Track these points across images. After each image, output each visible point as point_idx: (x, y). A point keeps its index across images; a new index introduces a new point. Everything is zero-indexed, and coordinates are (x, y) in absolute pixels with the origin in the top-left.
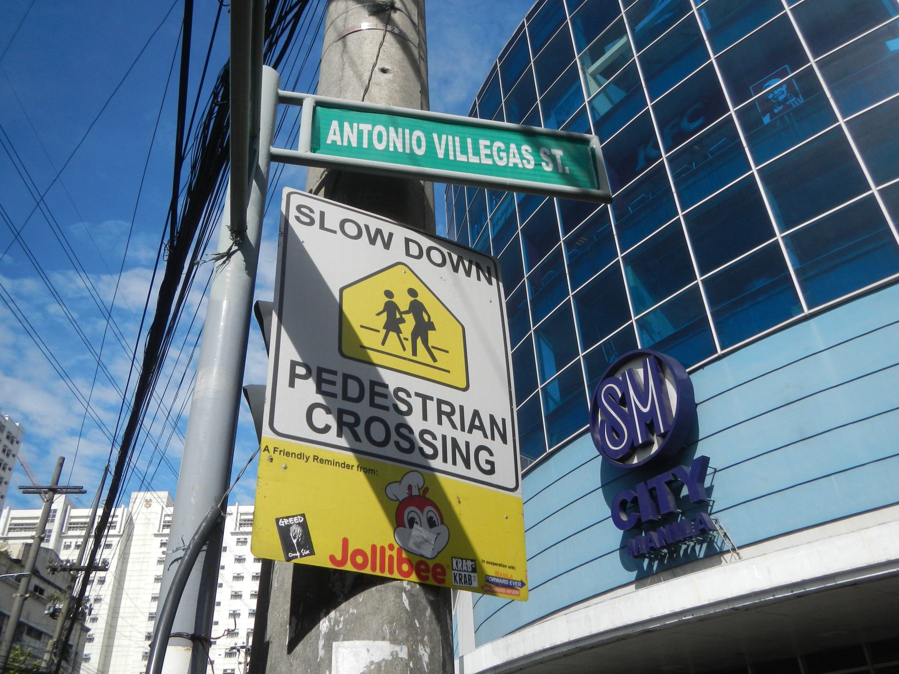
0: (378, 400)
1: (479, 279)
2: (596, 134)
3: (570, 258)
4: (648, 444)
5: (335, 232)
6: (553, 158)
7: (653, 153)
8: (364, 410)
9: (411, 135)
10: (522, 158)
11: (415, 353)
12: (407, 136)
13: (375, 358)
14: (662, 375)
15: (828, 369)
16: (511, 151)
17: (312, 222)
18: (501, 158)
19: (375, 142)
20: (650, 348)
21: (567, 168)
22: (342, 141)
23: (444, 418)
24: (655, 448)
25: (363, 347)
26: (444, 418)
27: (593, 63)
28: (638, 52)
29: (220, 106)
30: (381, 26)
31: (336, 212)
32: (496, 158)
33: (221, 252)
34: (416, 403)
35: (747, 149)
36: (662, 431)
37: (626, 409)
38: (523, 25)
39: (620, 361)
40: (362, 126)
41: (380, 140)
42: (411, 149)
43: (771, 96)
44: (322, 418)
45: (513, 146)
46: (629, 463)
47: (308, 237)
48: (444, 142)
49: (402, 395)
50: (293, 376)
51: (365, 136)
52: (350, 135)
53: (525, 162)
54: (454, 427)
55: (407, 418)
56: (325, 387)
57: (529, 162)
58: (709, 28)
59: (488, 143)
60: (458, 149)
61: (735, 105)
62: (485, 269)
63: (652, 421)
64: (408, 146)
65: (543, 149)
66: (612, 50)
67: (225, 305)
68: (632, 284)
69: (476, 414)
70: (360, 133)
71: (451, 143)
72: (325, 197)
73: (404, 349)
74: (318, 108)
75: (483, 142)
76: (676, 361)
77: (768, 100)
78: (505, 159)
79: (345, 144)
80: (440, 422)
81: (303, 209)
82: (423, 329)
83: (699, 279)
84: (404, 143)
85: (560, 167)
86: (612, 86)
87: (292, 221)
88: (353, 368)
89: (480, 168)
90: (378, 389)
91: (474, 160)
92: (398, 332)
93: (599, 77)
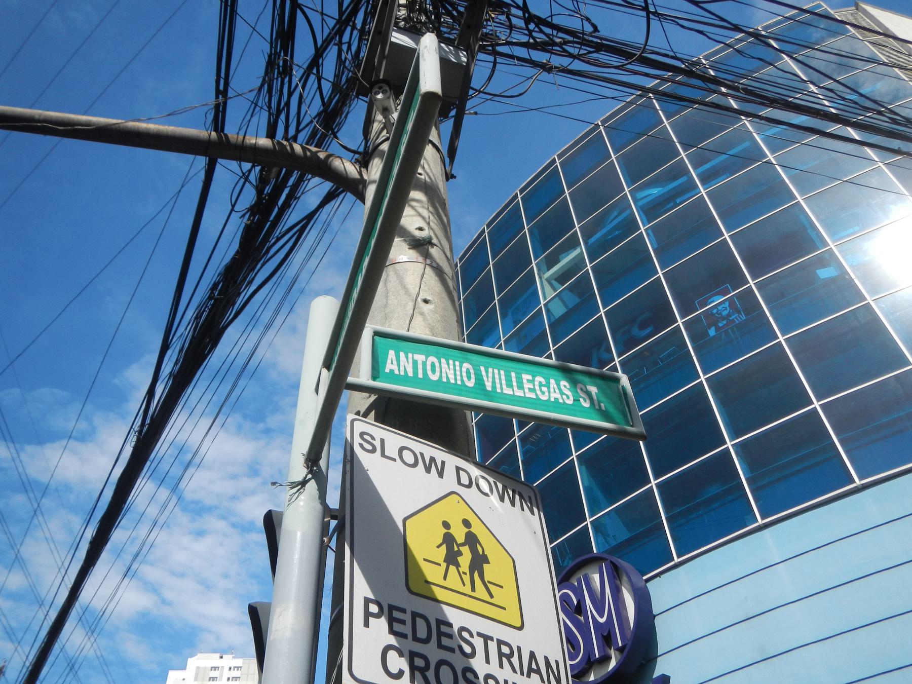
0: (445, 641)
1: (523, 509)
2: (624, 372)
3: (524, 454)
4: (606, 659)
5: (394, 460)
6: (589, 394)
7: (606, 356)
8: (432, 652)
9: (461, 367)
10: (562, 393)
11: (473, 589)
12: (458, 368)
13: (440, 594)
14: (618, 582)
15: (785, 583)
16: (551, 386)
17: (373, 451)
18: (543, 393)
19: (429, 373)
20: (606, 552)
21: (602, 405)
22: (399, 370)
23: (504, 660)
24: (613, 664)
25: (427, 582)
26: (504, 660)
27: (548, 270)
28: (591, 263)
29: (216, 300)
30: (421, 259)
31: (394, 439)
32: (539, 393)
33: (297, 480)
34: (478, 643)
35: (695, 358)
36: (620, 645)
37: (582, 618)
38: (483, 231)
39: (575, 565)
40: (416, 357)
41: (434, 371)
42: (462, 380)
43: (715, 311)
44: (397, 662)
45: (552, 381)
46: (585, 679)
47: (368, 461)
48: (490, 375)
49: (465, 635)
50: (367, 615)
51: (420, 366)
52: (406, 364)
53: (564, 397)
54: (514, 671)
55: (471, 660)
56: (397, 627)
57: (568, 397)
58: (656, 247)
59: (530, 377)
60: (504, 382)
61: (682, 318)
62: (527, 499)
63: (609, 633)
64: (459, 378)
65: (579, 385)
66: (566, 260)
67: (299, 534)
68: (587, 484)
69: (532, 655)
70: (415, 363)
71: (497, 376)
72: (375, 421)
73: (464, 585)
74: (376, 337)
75: (526, 377)
76: (632, 567)
77: (713, 315)
78: (547, 394)
79: (402, 373)
80: (501, 666)
81: (365, 437)
82: (479, 562)
83: (653, 483)
84: (455, 375)
85: (596, 402)
86: (566, 291)
87: (357, 449)
88: (420, 605)
89: (523, 401)
90: (444, 629)
91: (519, 393)
92: (457, 565)
93: (554, 282)
